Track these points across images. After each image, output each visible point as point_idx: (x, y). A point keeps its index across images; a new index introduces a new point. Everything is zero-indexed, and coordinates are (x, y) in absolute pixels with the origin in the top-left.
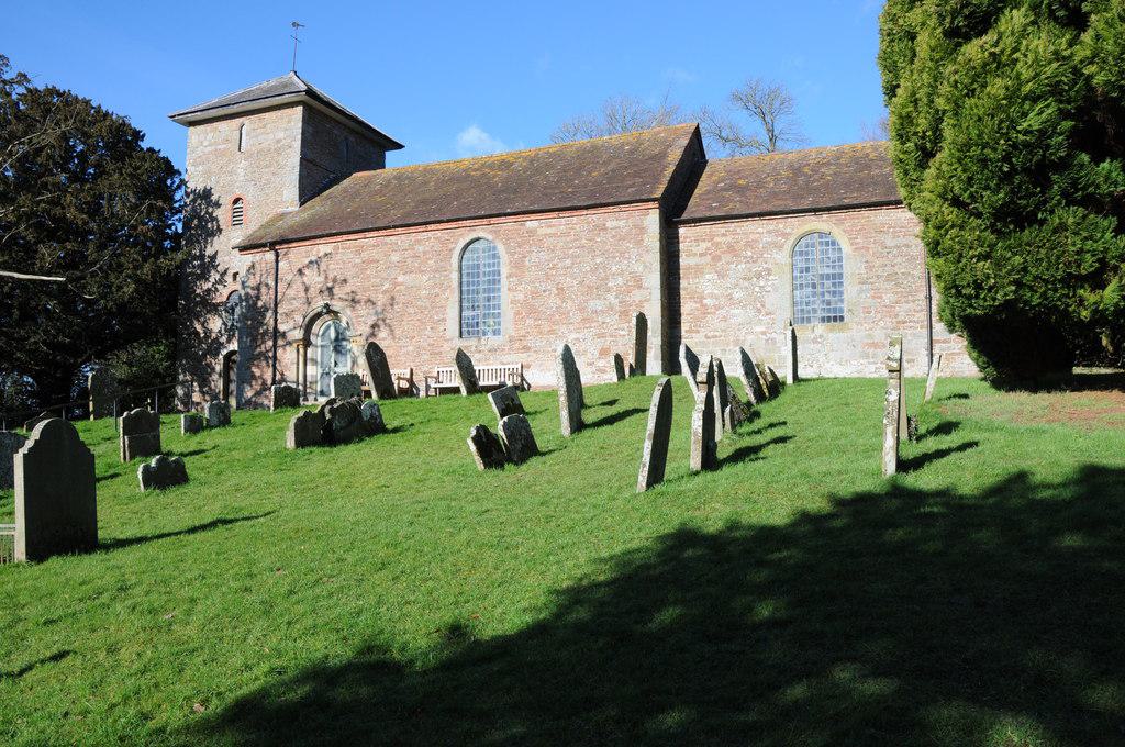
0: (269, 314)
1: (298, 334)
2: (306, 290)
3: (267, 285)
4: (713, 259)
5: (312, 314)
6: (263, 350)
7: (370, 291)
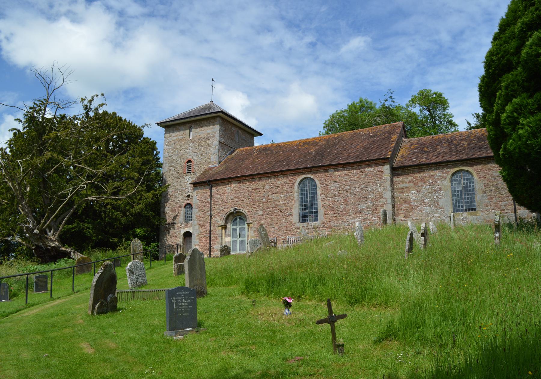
4: (414, 184)
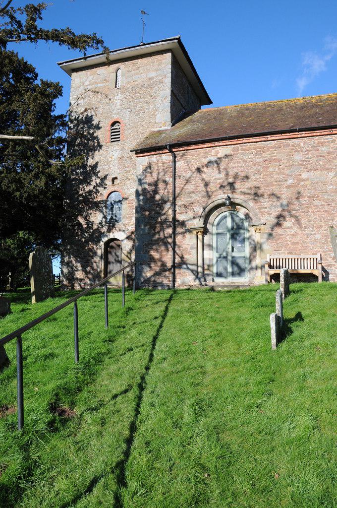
0: (168, 206)
1: (198, 223)
2: (206, 185)
3: (165, 181)
5: (212, 205)
6: (162, 236)
7: (273, 185)
